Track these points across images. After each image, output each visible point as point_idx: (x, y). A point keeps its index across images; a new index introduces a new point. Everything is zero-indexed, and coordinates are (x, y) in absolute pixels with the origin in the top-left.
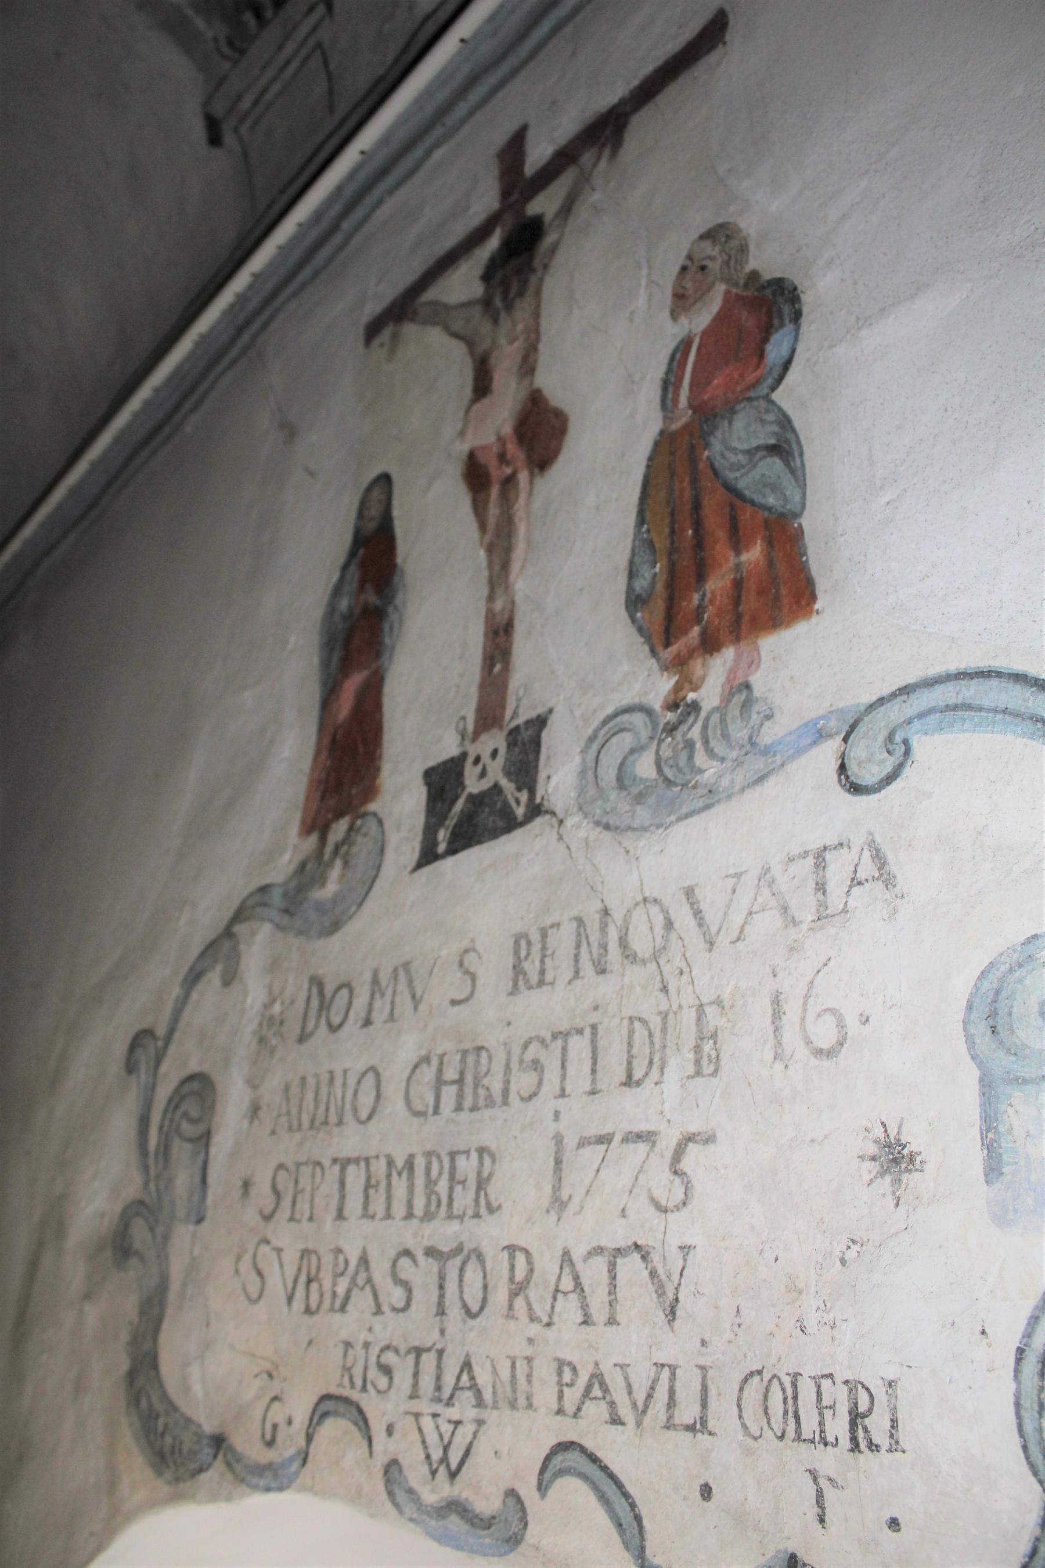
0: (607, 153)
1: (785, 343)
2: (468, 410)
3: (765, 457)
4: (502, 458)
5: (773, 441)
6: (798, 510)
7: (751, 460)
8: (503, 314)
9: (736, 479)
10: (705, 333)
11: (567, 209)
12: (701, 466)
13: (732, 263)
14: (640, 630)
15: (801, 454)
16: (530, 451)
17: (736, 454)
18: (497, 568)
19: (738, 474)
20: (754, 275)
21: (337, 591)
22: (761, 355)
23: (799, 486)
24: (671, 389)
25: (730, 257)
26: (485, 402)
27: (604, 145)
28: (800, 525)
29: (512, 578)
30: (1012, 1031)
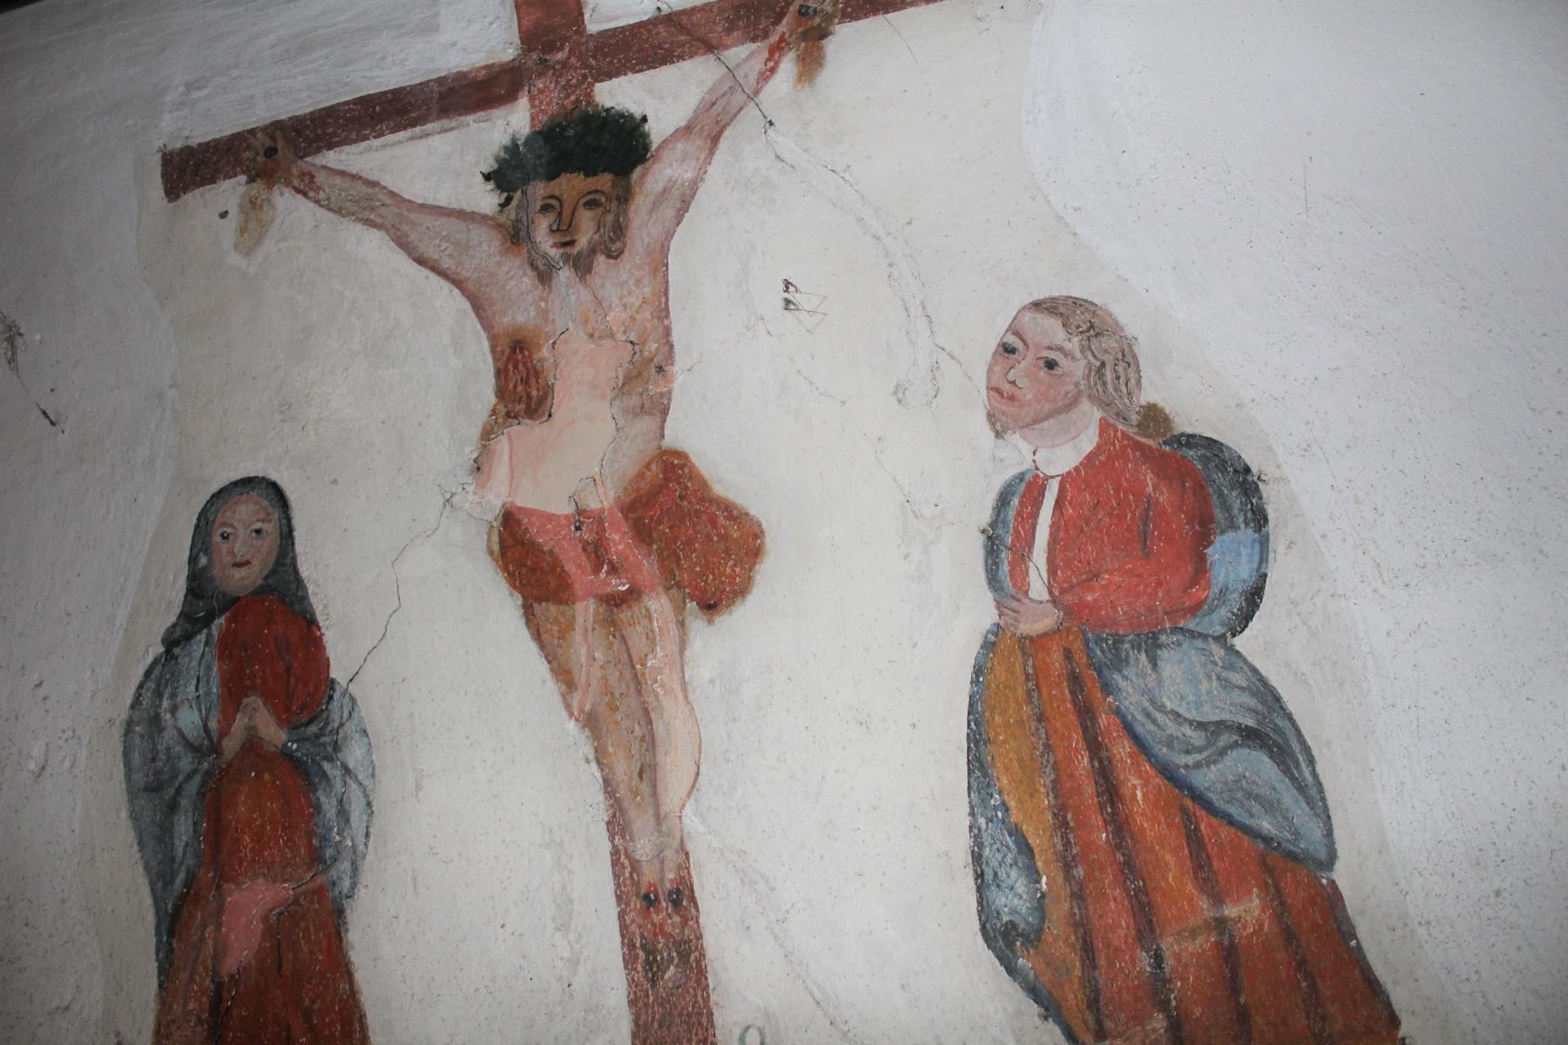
0: (788, 66)
1: (1244, 558)
2: (487, 434)
3: (1235, 746)
4: (596, 552)
5: (1251, 723)
6: (1322, 854)
7: (1209, 744)
8: (565, 275)
9: (1186, 766)
10: (1065, 479)
11: (709, 129)
12: (1103, 720)
13: (1109, 376)
14: (1033, 992)
15: (1311, 761)
16: (669, 563)
17: (1180, 724)
18: (623, 769)
19: (1190, 760)
20: (1154, 417)
21: (162, 675)
22: (1201, 568)
23: (1317, 815)
24: (1005, 556)
25: (1103, 364)
26: (524, 433)
27: (776, 51)
28: (1332, 883)
29: (670, 803)
30: (256, 503)
